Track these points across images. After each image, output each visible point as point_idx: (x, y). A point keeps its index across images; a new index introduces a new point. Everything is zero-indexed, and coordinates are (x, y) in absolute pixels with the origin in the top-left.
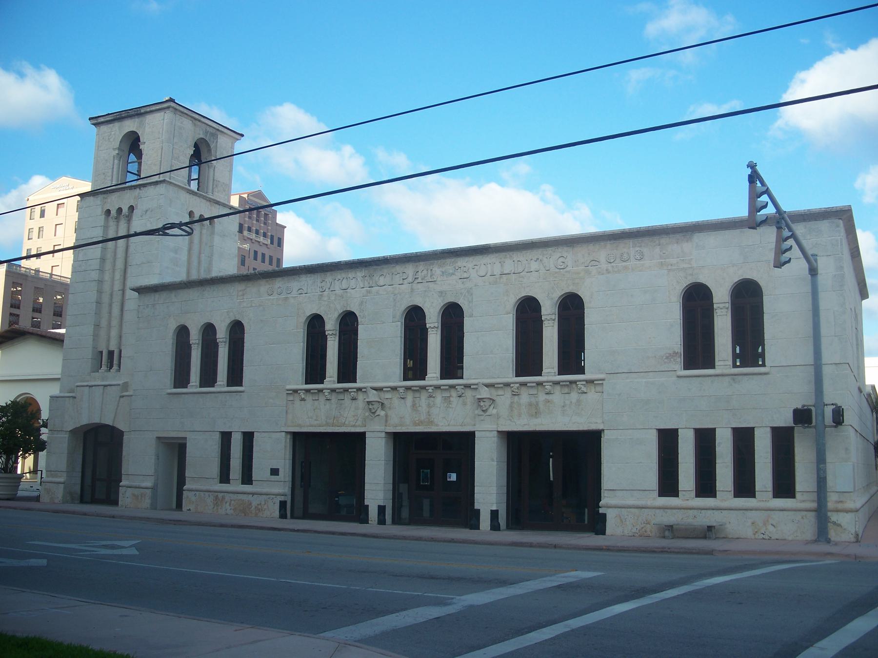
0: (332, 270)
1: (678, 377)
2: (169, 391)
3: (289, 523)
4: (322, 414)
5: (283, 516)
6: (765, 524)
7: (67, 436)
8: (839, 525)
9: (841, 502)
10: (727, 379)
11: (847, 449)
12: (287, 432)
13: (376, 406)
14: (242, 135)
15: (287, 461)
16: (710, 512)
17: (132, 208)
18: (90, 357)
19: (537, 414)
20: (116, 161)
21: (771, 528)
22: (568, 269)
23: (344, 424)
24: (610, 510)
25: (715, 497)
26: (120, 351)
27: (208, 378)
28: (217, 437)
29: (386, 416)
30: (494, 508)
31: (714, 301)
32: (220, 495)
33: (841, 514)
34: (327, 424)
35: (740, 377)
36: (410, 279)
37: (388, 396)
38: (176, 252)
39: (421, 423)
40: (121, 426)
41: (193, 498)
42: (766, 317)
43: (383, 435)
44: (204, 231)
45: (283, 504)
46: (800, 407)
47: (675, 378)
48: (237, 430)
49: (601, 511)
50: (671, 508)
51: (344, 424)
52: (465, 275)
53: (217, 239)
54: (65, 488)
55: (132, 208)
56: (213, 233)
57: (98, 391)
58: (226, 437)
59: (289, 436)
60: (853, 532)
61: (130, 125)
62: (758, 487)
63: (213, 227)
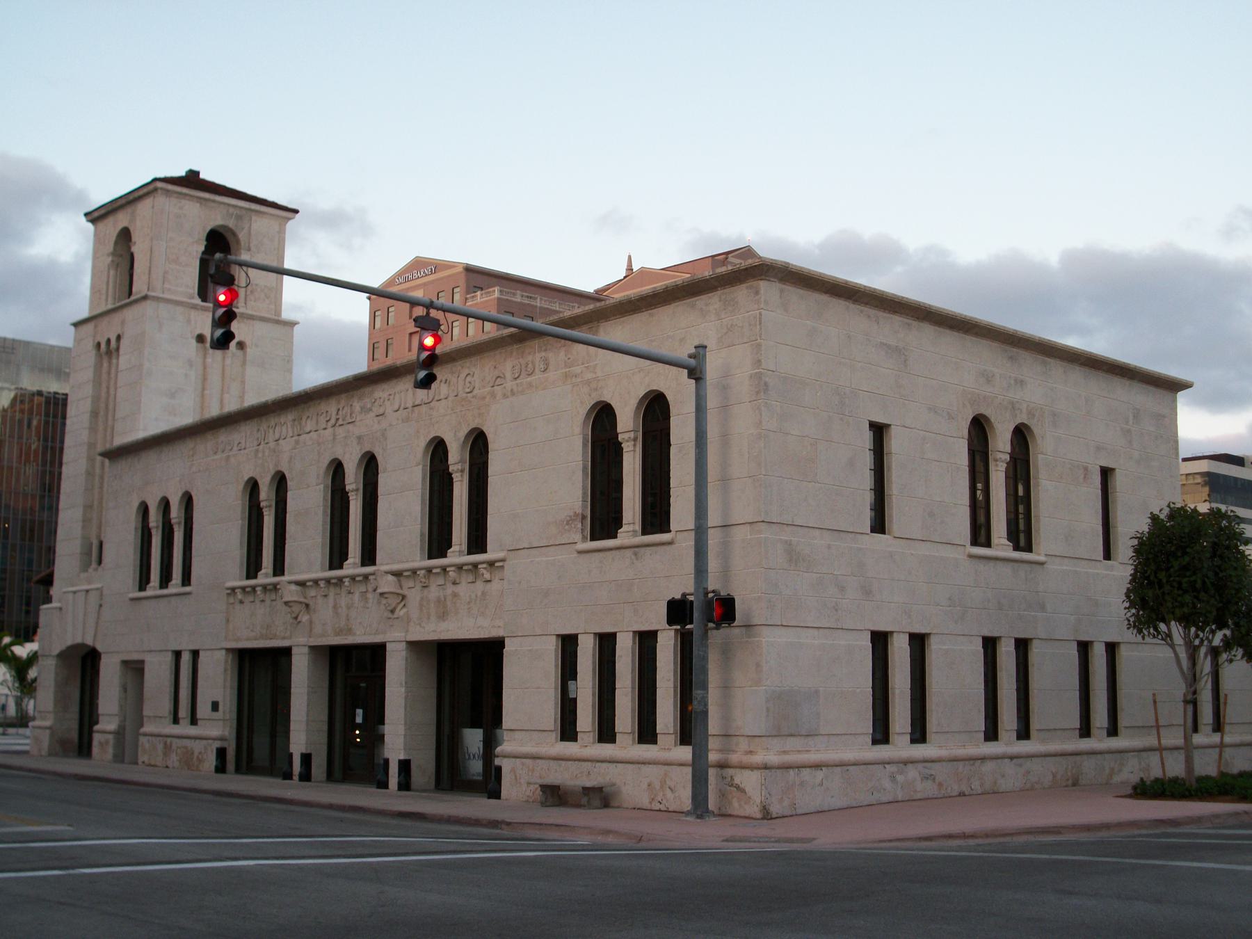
0: (274, 412)
1: (580, 552)
2: (131, 595)
3: (235, 783)
4: (255, 627)
5: (221, 768)
6: (662, 787)
7: (54, 662)
8: (743, 791)
9: (751, 752)
10: (628, 553)
11: (758, 665)
12: (228, 650)
13: (296, 608)
14: (296, 212)
15: (228, 690)
16: (604, 765)
17: (119, 338)
18: (78, 551)
19: (443, 616)
20: (112, 272)
21: (668, 792)
22: (475, 392)
23: (238, 640)
24: (505, 760)
25: (614, 741)
26: (101, 544)
27: (165, 580)
28: (169, 658)
29: (311, 622)
30: (402, 757)
31: (619, 430)
32: (169, 740)
33: (747, 773)
34: (263, 637)
35: (643, 550)
36: (333, 421)
37: (312, 593)
38: (172, 395)
39: (339, 632)
40: (99, 648)
41: (147, 745)
42: (673, 451)
43: (306, 650)
44: (228, 361)
45: (221, 753)
46: (678, 596)
47: (576, 555)
48: (186, 645)
49: (497, 762)
50: (602, 761)
51: (274, 637)
52: (381, 411)
53: (251, 371)
54: (52, 735)
55: (119, 338)
56: (244, 363)
57: (71, 596)
58: (569, 644)
59: (231, 656)
60: (758, 801)
61: (121, 220)
62: (660, 728)
63: (245, 355)
